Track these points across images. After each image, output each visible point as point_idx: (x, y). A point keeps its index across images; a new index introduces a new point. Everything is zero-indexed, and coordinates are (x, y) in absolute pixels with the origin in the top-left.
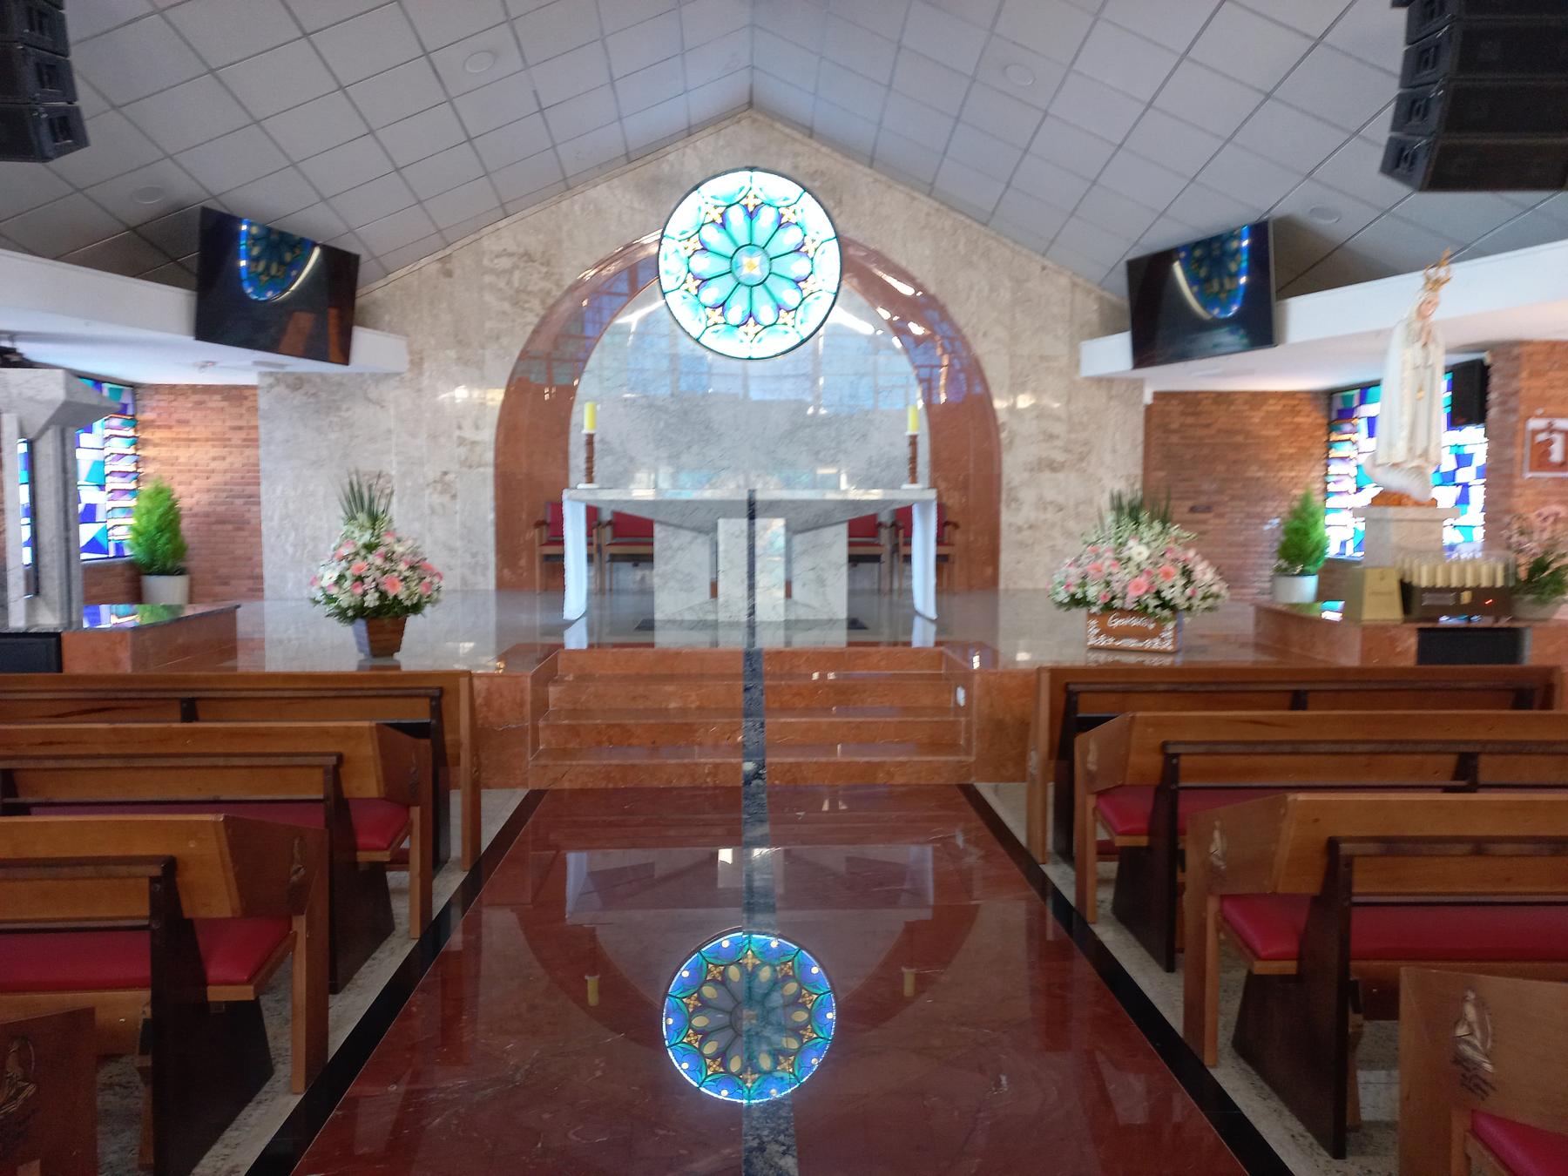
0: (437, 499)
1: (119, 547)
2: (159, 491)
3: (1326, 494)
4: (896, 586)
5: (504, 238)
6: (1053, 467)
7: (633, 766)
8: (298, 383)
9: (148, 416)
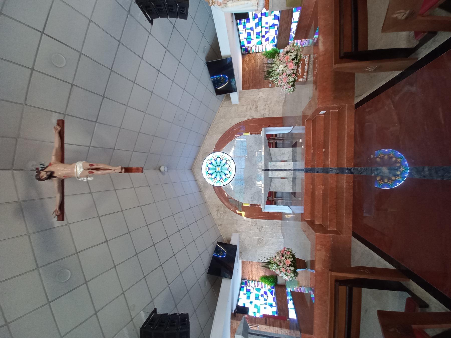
0: (263, 230)
1: (272, 288)
2: (261, 279)
3: (262, 52)
4: (281, 138)
5: (214, 214)
6: (257, 107)
7: (346, 206)
8: (241, 253)
9: (247, 278)
